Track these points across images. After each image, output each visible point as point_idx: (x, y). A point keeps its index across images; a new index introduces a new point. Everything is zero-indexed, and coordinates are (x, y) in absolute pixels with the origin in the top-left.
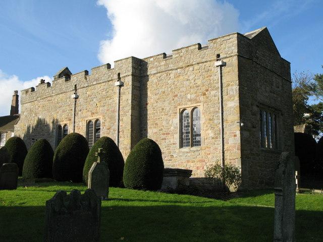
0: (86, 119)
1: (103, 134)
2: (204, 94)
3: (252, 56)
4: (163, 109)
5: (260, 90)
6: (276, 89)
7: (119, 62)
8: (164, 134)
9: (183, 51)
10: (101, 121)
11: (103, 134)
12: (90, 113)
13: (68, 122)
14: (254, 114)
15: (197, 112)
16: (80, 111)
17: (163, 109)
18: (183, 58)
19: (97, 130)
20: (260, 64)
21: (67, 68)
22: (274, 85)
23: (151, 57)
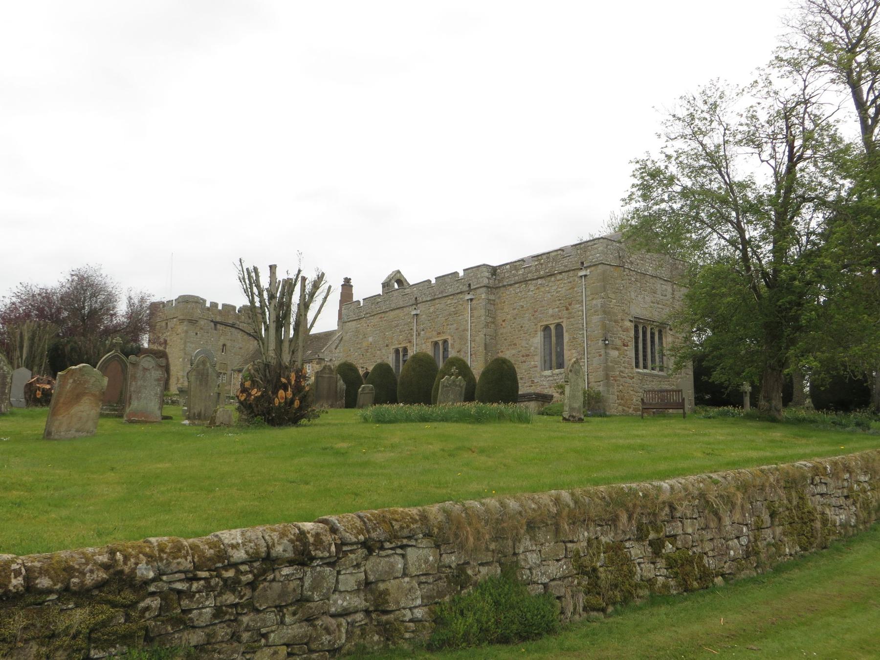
0: (432, 340)
1: (452, 354)
2: (567, 309)
3: (624, 262)
4: (522, 327)
5: (634, 301)
6: (662, 297)
7: (470, 271)
8: (523, 356)
9: (544, 257)
10: (450, 342)
11: (452, 354)
12: (435, 333)
13: (408, 345)
14: (627, 330)
15: (248, 296)
16: (423, 330)
17: (522, 327)
18: (544, 266)
19: (445, 350)
20: (634, 271)
21: (399, 272)
22: (659, 292)
23: (507, 264)
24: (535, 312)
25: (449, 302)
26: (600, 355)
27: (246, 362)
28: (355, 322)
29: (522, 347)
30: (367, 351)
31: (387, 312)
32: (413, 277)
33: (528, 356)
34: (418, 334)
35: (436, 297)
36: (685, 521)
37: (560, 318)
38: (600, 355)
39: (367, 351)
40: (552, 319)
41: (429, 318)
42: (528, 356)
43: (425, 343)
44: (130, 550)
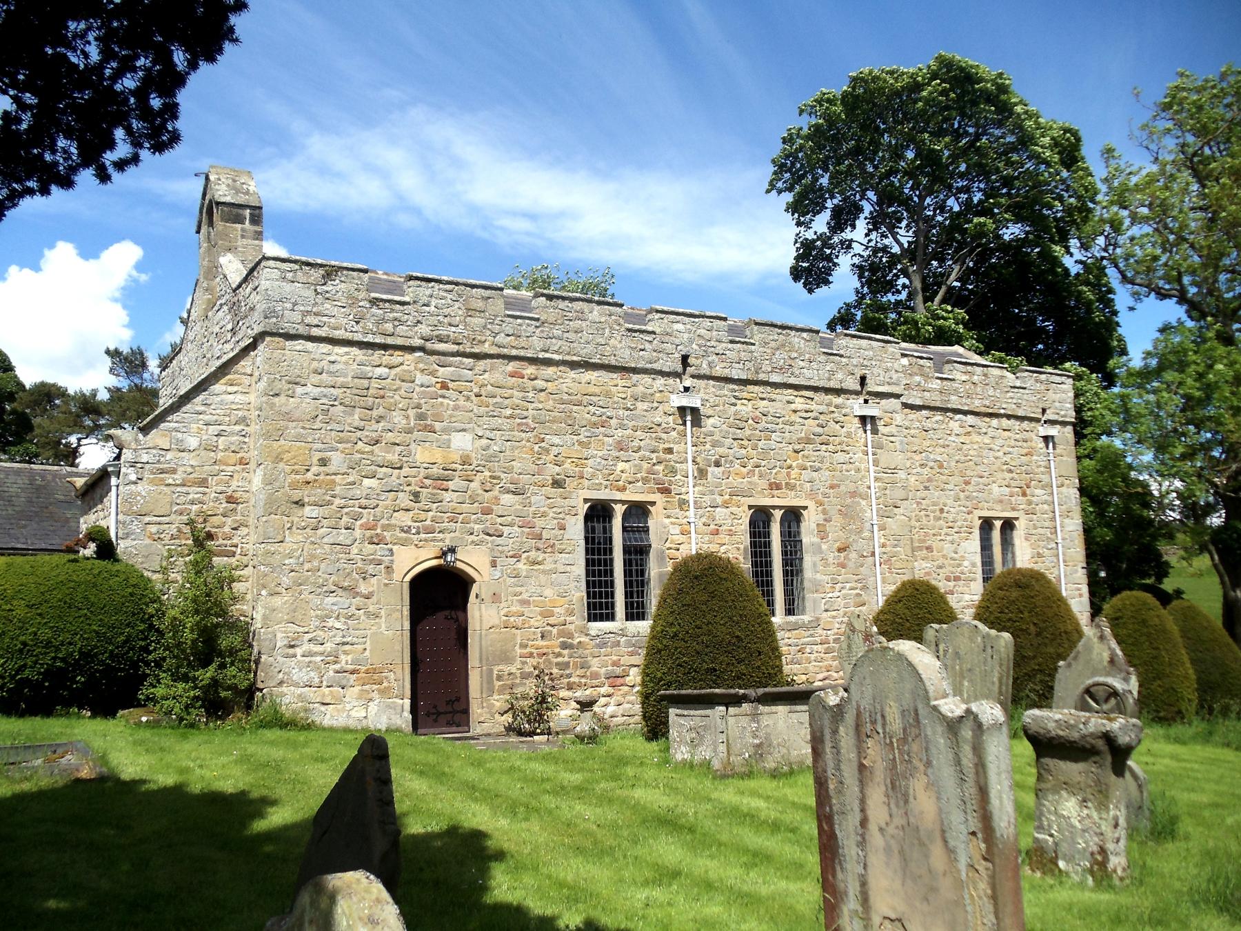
2: (1024, 494)
4: (942, 511)
8: (948, 579)
12: (763, 484)
16: (717, 464)
24: (967, 483)
25: (799, 404)
26: (1081, 595)
27: (84, 717)
28: (355, 351)
29: (944, 556)
30: (441, 481)
31: (548, 362)
32: (126, 320)
33: (957, 579)
34: (702, 473)
35: (762, 377)
36: (510, 714)
37: (1013, 509)
38: (1081, 595)
39: (441, 481)
40: (998, 507)
41: (739, 433)
42: (957, 579)
43: (726, 505)
44: (82, 26)
